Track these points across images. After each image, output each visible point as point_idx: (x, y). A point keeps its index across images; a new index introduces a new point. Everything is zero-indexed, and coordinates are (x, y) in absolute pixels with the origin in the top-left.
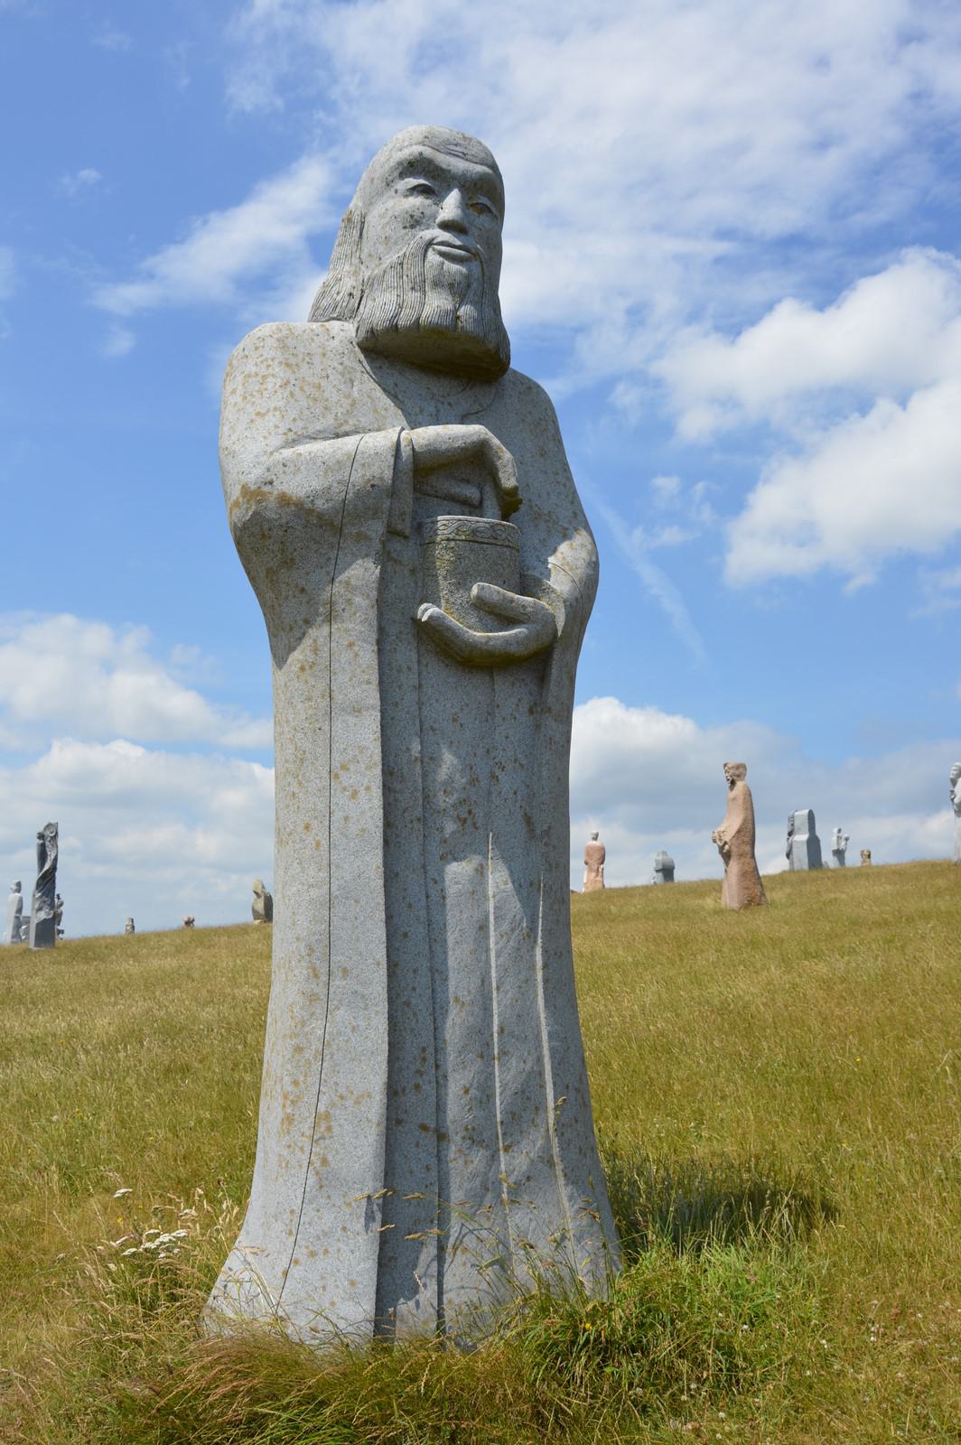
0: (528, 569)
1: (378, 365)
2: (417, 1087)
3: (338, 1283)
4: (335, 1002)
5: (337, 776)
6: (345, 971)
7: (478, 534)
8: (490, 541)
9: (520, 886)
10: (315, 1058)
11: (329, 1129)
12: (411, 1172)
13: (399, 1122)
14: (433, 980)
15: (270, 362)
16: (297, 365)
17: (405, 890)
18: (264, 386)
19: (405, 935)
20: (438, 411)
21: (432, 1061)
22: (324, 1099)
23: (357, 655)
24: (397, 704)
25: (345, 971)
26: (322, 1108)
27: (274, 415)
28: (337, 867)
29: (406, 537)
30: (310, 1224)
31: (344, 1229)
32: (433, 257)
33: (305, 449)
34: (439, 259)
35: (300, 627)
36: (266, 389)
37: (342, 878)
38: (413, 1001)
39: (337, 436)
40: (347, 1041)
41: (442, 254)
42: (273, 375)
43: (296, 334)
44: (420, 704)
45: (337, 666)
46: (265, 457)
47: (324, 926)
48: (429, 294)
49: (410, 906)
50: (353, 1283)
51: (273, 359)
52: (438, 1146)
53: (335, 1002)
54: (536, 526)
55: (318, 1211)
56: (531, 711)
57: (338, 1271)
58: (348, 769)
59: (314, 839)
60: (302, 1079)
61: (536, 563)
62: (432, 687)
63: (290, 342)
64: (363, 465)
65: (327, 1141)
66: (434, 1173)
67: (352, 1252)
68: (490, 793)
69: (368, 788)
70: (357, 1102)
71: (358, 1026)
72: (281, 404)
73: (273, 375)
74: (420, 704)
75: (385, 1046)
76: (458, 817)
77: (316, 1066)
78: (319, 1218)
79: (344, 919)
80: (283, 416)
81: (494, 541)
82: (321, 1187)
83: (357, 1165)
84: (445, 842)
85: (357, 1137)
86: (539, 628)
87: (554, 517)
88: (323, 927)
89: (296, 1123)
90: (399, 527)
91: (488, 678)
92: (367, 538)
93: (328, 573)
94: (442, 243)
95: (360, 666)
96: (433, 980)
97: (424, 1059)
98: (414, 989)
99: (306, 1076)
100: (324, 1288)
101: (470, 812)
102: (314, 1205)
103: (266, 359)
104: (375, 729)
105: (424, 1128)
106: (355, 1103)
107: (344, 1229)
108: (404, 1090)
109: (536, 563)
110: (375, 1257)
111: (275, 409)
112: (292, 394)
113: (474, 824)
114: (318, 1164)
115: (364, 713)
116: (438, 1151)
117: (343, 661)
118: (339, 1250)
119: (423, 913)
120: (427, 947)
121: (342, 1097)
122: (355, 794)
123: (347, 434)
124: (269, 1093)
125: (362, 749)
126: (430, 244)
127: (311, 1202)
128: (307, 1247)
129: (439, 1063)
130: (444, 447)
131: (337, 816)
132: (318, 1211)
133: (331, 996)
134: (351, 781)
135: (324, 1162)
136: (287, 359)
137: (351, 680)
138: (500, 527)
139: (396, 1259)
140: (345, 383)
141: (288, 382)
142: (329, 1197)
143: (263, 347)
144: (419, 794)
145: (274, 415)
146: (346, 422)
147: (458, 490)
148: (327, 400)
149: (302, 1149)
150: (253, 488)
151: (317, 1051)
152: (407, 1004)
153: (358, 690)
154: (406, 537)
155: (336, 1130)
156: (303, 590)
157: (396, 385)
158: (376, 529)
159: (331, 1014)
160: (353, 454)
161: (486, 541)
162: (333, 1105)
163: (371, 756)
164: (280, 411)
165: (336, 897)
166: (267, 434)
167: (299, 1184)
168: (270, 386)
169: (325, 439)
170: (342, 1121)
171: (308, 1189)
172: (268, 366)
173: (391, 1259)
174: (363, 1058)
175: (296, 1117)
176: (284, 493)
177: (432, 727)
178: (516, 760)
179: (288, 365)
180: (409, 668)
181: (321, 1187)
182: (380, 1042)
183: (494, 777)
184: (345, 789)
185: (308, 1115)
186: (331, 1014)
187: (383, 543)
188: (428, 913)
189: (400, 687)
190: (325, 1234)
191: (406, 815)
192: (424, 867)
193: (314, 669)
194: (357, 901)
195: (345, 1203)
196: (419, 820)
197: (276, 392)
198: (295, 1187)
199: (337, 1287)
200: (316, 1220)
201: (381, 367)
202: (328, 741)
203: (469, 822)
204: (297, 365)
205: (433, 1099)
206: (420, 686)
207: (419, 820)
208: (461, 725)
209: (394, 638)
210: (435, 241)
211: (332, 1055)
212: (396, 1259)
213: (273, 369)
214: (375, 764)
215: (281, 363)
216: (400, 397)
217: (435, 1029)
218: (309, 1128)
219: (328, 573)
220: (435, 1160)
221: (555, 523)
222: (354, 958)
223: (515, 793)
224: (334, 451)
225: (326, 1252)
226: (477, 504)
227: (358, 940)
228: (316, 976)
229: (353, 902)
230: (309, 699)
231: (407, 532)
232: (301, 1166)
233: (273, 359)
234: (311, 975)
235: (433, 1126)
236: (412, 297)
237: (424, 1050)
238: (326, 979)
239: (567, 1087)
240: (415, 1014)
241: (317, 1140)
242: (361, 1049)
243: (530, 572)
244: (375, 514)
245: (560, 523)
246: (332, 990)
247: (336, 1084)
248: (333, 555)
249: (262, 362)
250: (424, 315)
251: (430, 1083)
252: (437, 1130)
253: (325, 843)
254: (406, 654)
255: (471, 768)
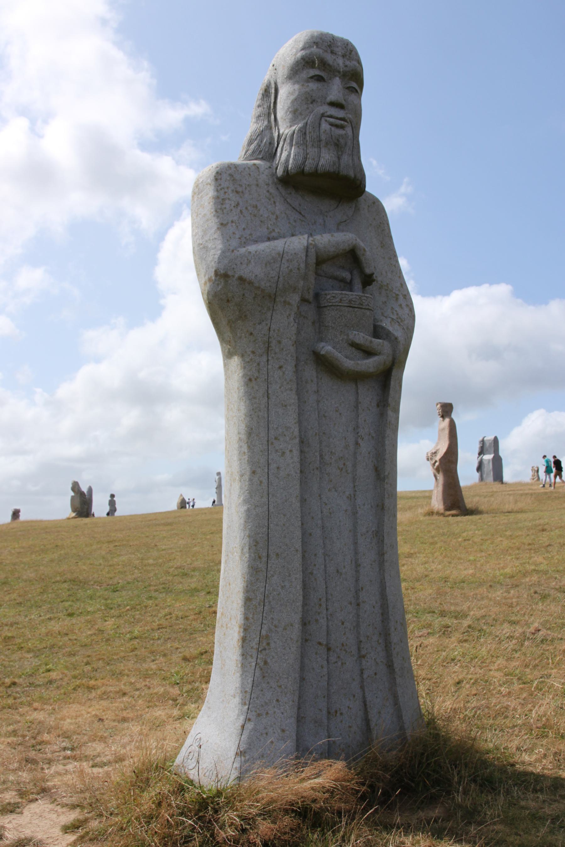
0: (378, 322)
1: (289, 192)
2: (317, 621)
3: (275, 731)
4: (271, 573)
5: (272, 443)
6: (277, 555)
7: (353, 302)
8: (359, 306)
9: (372, 507)
10: (259, 604)
11: (268, 644)
12: (313, 669)
13: (306, 640)
14: (325, 560)
15: (226, 190)
16: (242, 192)
17: (310, 509)
18: (224, 206)
19: (310, 534)
20: (325, 221)
21: (325, 606)
22: (265, 627)
23: (284, 373)
24: (305, 402)
25: (277, 555)
26: (264, 632)
27: (232, 226)
28: (273, 495)
29: (310, 303)
30: (257, 698)
31: (277, 700)
32: (325, 126)
33: (252, 248)
34: (328, 127)
35: (249, 355)
36: (225, 208)
37: (276, 502)
38: (315, 572)
39: (269, 239)
40: (278, 594)
41: (332, 124)
42: (229, 199)
43: (240, 171)
44: (318, 402)
45: (272, 379)
46: (229, 254)
47: (265, 529)
48: (323, 150)
49: (313, 518)
50: (283, 731)
51: (228, 188)
52: (328, 654)
53: (271, 573)
54: (380, 293)
55: (262, 691)
56: (378, 406)
57: (275, 724)
58: (279, 440)
59: (259, 480)
60: (251, 616)
61: (382, 318)
62: (324, 391)
63: (237, 177)
64: (288, 260)
65: (267, 651)
66: (325, 670)
67: (282, 713)
68: (355, 453)
69: (291, 451)
70: (285, 629)
71: (285, 586)
72: (236, 218)
73: (229, 199)
74: (318, 402)
75: (301, 598)
76: (338, 467)
77: (260, 609)
78: (263, 695)
79: (277, 525)
80: (237, 226)
81: (361, 306)
82: (264, 677)
83: (285, 665)
84: (331, 481)
85: (284, 649)
86: (385, 357)
87: (390, 287)
88: (264, 529)
89: (247, 641)
90: (307, 297)
91: (354, 386)
92: (289, 304)
93: (267, 324)
94: (331, 117)
95: (286, 380)
96: (325, 560)
97: (320, 605)
98: (315, 565)
99: (254, 614)
100: (267, 734)
101: (344, 464)
102: (260, 688)
103: (223, 188)
104: (295, 417)
105: (320, 643)
106: (284, 629)
107: (277, 700)
108: (309, 622)
109: (382, 318)
110: (295, 716)
111: (232, 222)
112: (241, 211)
113: (347, 471)
114: (262, 664)
115: (288, 407)
116: (328, 657)
117: (276, 376)
118: (275, 712)
119: (320, 522)
120: (322, 541)
121: (276, 626)
122: (283, 453)
123: (275, 239)
124: (225, 625)
125: (288, 428)
126: (323, 115)
127: (257, 686)
128: (256, 711)
129: (328, 607)
130: (333, 249)
131: (273, 466)
132: (262, 691)
133: (269, 569)
134: (281, 446)
135: (266, 663)
136: (236, 188)
137: (280, 388)
138: (364, 298)
139: (305, 718)
140: (271, 204)
141: (238, 204)
142: (268, 683)
143: (221, 179)
144: (317, 454)
145: (232, 226)
146: (274, 230)
147: (338, 273)
148: (262, 216)
149: (251, 656)
150: (222, 272)
151: (260, 600)
152: (312, 573)
153: (285, 394)
154: (310, 303)
155: (272, 645)
156: (251, 334)
157: (300, 205)
158: (295, 299)
159: (269, 579)
160: (282, 253)
161: (356, 306)
162: (270, 630)
163: (293, 433)
164: (236, 223)
165: (272, 512)
166: (229, 239)
167: (250, 676)
168: (227, 206)
169: (263, 241)
170: (276, 640)
171: (256, 679)
172: (225, 193)
173: (302, 718)
174: (288, 604)
175: (247, 638)
176: (241, 276)
177: (324, 415)
178: (370, 434)
179: (237, 192)
180: (312, 381)
181: (264, 677)
182: (298, 595)
183: (357, 444)
184: (277, 451)
185: (255, 636)
186: (269, 579)
187: (298, 307)
188: (322, 522)
189: (307, 392)
190: (266, 703)
191: (310, 466)
192: (320, 496)
193: (258, 380)
194: (285, 515)
195: (278, 686)
196: (317, 469)
197: (231, 210)
198: (247, 678)
199: (274, 733)
200: (261, 696)
201: (290, 193)
202: (266, 423)
203: (344, 470)
204: (242, 192)
205: (325, 628)
206: (318, 391)
207: (317, 469)
208: (340, 414)
209: (303, 363)
210: (326, 114)
211: (270, 602)
212: (305, 718)
213: (229, 194)
214: (295, 437)
215: (233, 191)
216: (302, 213)
217: (326, 588)
218: (256, 644)
219: (267, 324)
220: (326, 662)
221: (391, 291)
222: (283, 547)
223: (369, 453)
224: (271, 251)
225: (267, 713)
226: (349, 281)
227: (285, 537)
228: (260, 557)
229: (282, 515)
230: (255, 398)
231: (311, 300)
232: (251, 666)
233: (228, 188)
234: (257, 557)
235: (325, 643)
236: (313, 152)
237: (320, 599)
238: (266, 559)
239: (397, 622)
240: (316, 579)
241: (261, 651)
242: (287, 599)
243: (379, 323)
244: (295, 289)
245: (394, 291)
246: (269, 565)
247: (272, 619)
248: (269, 314)
249: (221, 189)
250: (320, 164)
251: (323, 618)
252: (327, 645)
253: (265, 482)
254: (310, 372)
255: (345, 439)
